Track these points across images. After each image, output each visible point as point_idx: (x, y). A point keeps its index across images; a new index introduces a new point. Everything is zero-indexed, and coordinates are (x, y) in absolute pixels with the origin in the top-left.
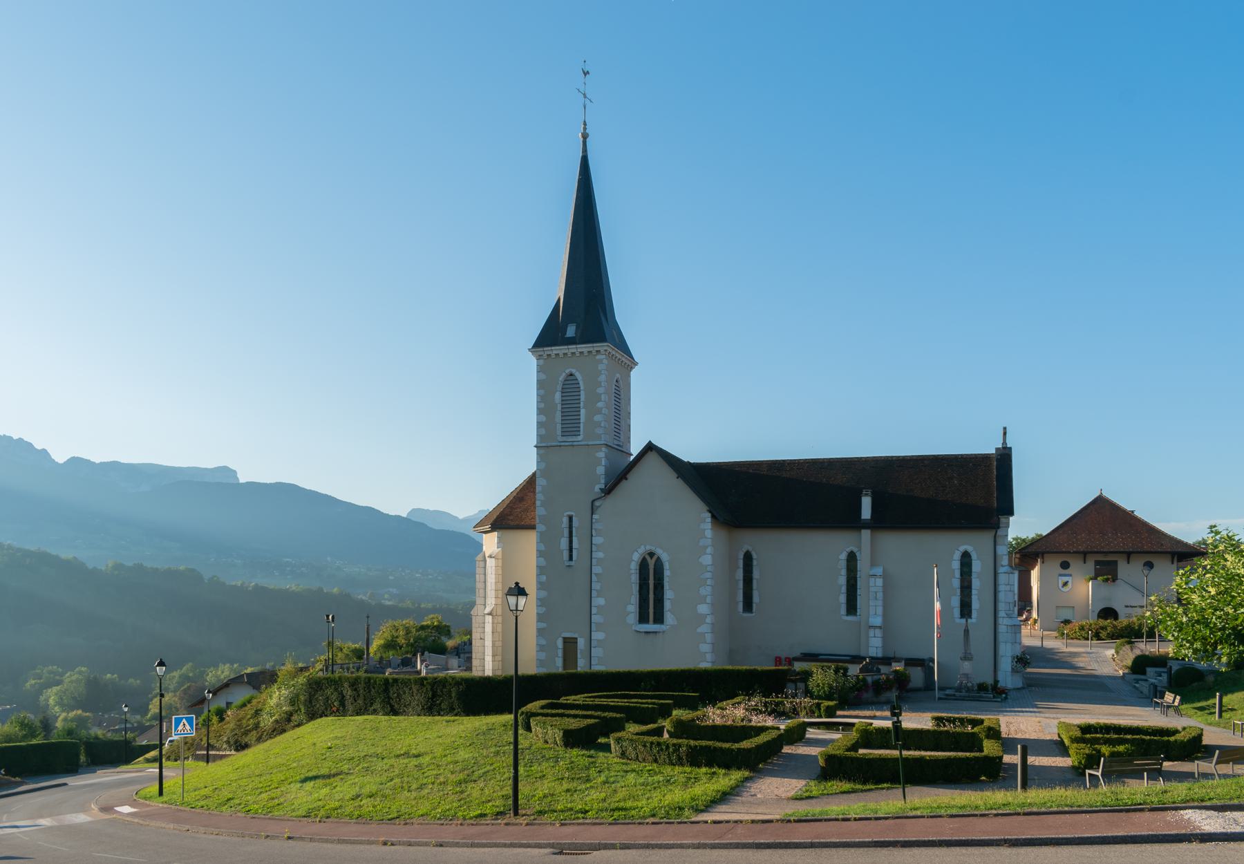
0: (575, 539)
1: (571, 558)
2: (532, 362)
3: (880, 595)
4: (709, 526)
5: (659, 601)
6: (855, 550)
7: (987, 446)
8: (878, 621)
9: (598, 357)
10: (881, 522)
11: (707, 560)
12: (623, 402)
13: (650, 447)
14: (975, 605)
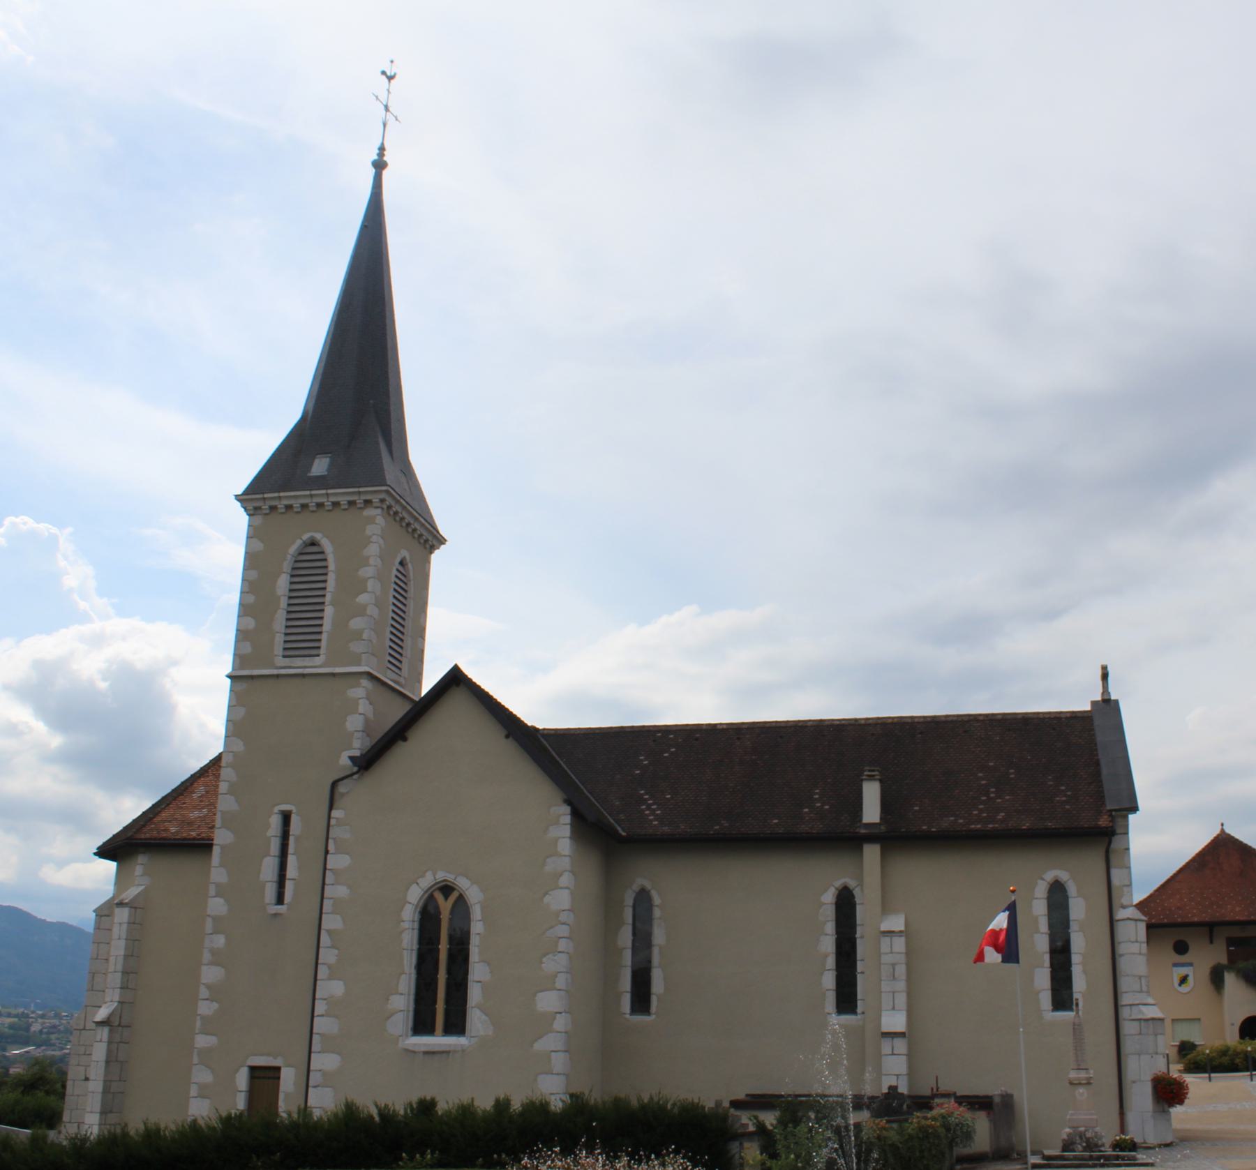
0: (292, 860)
1: (280, 900)
2: (240, 520)
3: (901, 970)
4: (567, 831)
6: (852, 883)
7: (1076, 698)
8: (895, 1021)
9: (369, 512)
10: (897, 837)
11: (560, 899)
12: (411, 604)
13: (455, 679)
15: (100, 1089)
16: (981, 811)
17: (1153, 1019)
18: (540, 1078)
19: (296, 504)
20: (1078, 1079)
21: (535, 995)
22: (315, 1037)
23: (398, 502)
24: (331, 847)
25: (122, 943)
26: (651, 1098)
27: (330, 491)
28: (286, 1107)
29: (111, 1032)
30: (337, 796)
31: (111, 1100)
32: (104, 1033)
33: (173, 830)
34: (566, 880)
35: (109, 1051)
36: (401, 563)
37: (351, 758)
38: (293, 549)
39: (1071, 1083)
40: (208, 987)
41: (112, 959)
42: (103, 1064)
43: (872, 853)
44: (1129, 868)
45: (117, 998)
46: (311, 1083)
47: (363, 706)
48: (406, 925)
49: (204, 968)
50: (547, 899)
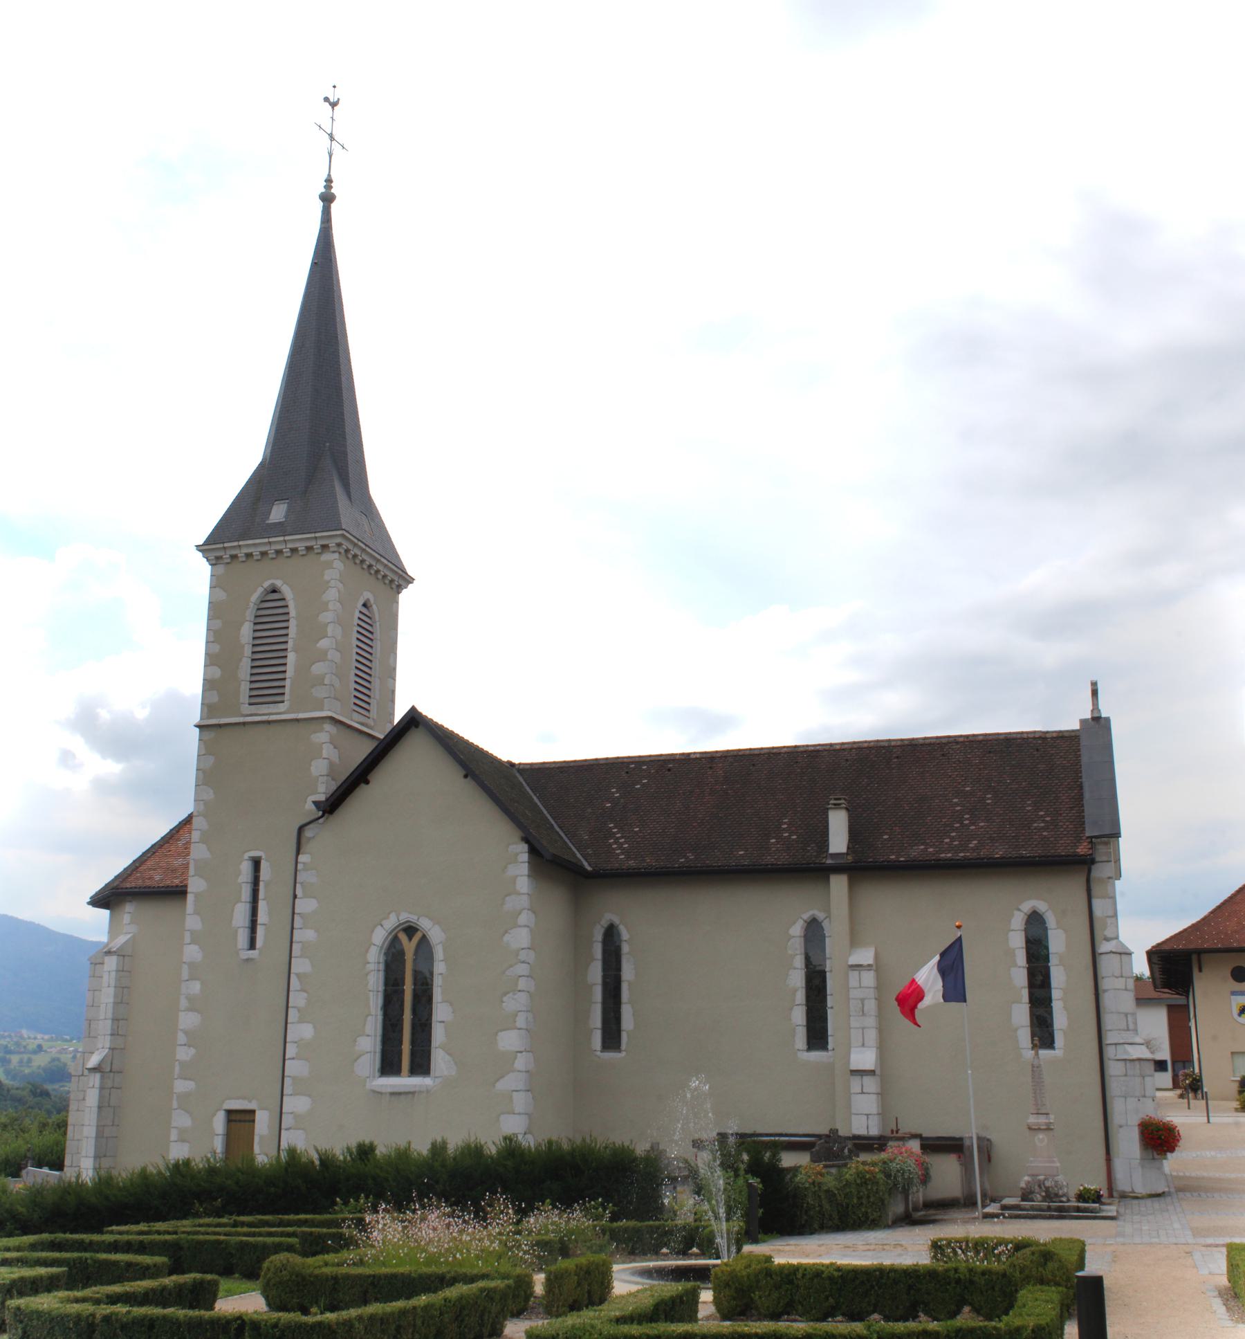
0: (262, 906)
1: (252, 945)
2: (202, 570)
3: (871, 1005)
5: (423, 1027)
6: (820, 916)
8: (865, 1058)
9: (326, 557)
10: (864, 867)
11: (520, 938)
12: (378, 645)
14: (1060, 1020)
15: (94, 1135)
16: (952, 839)
17: (1140, 1060)
18: (502, 1117)
19: (256, 552)
20: (1038, 1124)
21: (496, 1034)
22: (286, 1079)
23: (355, 545)
24: (299, 892)
25: (112, 990)
26: (584, 1140)
27: (287, 538)
28: (263, 1155)
29: (102, 1078)
30: (303, 841)
31: (105, 1144)
32: (96, 1079)
33: (157, 878)
34: (524, 918)
35: (101, 1097)
36: (365, 605)
37: (314, 803)
38: (255, 597)
39: (1030, 1128)
40: (186, 1033)
41: (103, 1007)
42: (95, 1110)
43: (839, 884)
44: (1114, 898)
45: (108, 1045)
46: (283, 1126)
47: (328, 751)
48: (371, 967)
49: (182, 1015)
50: (506, 938)
